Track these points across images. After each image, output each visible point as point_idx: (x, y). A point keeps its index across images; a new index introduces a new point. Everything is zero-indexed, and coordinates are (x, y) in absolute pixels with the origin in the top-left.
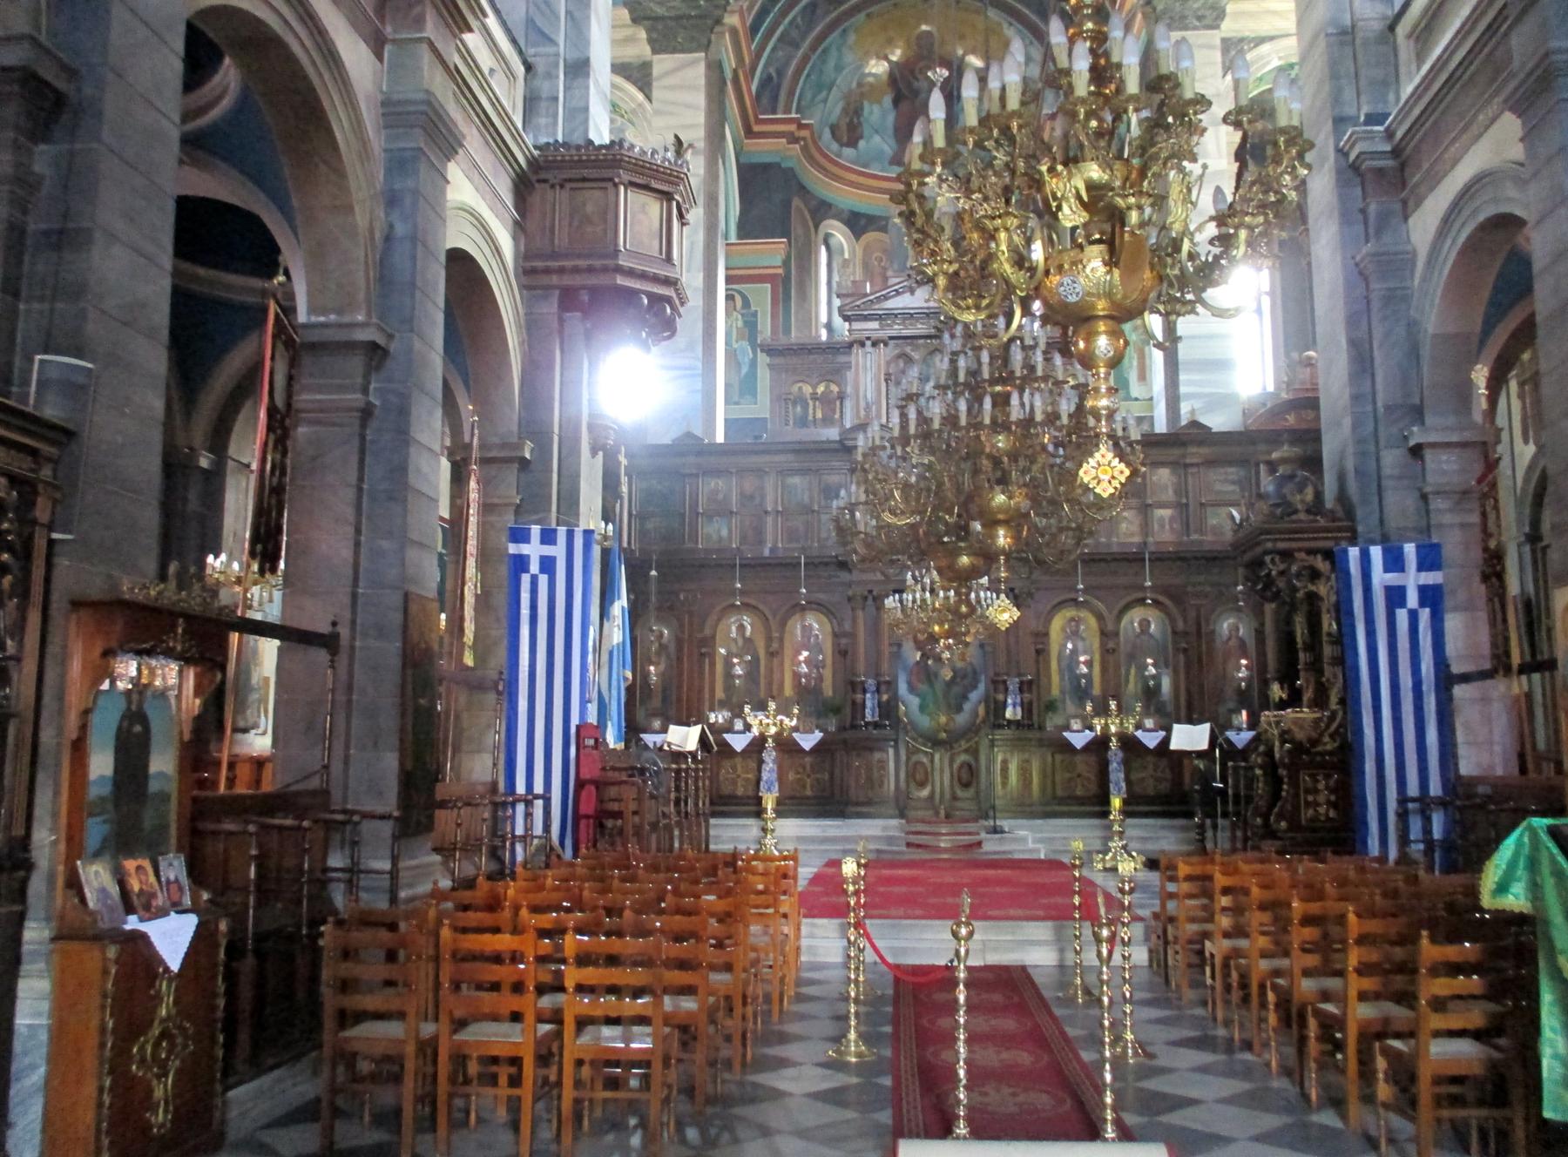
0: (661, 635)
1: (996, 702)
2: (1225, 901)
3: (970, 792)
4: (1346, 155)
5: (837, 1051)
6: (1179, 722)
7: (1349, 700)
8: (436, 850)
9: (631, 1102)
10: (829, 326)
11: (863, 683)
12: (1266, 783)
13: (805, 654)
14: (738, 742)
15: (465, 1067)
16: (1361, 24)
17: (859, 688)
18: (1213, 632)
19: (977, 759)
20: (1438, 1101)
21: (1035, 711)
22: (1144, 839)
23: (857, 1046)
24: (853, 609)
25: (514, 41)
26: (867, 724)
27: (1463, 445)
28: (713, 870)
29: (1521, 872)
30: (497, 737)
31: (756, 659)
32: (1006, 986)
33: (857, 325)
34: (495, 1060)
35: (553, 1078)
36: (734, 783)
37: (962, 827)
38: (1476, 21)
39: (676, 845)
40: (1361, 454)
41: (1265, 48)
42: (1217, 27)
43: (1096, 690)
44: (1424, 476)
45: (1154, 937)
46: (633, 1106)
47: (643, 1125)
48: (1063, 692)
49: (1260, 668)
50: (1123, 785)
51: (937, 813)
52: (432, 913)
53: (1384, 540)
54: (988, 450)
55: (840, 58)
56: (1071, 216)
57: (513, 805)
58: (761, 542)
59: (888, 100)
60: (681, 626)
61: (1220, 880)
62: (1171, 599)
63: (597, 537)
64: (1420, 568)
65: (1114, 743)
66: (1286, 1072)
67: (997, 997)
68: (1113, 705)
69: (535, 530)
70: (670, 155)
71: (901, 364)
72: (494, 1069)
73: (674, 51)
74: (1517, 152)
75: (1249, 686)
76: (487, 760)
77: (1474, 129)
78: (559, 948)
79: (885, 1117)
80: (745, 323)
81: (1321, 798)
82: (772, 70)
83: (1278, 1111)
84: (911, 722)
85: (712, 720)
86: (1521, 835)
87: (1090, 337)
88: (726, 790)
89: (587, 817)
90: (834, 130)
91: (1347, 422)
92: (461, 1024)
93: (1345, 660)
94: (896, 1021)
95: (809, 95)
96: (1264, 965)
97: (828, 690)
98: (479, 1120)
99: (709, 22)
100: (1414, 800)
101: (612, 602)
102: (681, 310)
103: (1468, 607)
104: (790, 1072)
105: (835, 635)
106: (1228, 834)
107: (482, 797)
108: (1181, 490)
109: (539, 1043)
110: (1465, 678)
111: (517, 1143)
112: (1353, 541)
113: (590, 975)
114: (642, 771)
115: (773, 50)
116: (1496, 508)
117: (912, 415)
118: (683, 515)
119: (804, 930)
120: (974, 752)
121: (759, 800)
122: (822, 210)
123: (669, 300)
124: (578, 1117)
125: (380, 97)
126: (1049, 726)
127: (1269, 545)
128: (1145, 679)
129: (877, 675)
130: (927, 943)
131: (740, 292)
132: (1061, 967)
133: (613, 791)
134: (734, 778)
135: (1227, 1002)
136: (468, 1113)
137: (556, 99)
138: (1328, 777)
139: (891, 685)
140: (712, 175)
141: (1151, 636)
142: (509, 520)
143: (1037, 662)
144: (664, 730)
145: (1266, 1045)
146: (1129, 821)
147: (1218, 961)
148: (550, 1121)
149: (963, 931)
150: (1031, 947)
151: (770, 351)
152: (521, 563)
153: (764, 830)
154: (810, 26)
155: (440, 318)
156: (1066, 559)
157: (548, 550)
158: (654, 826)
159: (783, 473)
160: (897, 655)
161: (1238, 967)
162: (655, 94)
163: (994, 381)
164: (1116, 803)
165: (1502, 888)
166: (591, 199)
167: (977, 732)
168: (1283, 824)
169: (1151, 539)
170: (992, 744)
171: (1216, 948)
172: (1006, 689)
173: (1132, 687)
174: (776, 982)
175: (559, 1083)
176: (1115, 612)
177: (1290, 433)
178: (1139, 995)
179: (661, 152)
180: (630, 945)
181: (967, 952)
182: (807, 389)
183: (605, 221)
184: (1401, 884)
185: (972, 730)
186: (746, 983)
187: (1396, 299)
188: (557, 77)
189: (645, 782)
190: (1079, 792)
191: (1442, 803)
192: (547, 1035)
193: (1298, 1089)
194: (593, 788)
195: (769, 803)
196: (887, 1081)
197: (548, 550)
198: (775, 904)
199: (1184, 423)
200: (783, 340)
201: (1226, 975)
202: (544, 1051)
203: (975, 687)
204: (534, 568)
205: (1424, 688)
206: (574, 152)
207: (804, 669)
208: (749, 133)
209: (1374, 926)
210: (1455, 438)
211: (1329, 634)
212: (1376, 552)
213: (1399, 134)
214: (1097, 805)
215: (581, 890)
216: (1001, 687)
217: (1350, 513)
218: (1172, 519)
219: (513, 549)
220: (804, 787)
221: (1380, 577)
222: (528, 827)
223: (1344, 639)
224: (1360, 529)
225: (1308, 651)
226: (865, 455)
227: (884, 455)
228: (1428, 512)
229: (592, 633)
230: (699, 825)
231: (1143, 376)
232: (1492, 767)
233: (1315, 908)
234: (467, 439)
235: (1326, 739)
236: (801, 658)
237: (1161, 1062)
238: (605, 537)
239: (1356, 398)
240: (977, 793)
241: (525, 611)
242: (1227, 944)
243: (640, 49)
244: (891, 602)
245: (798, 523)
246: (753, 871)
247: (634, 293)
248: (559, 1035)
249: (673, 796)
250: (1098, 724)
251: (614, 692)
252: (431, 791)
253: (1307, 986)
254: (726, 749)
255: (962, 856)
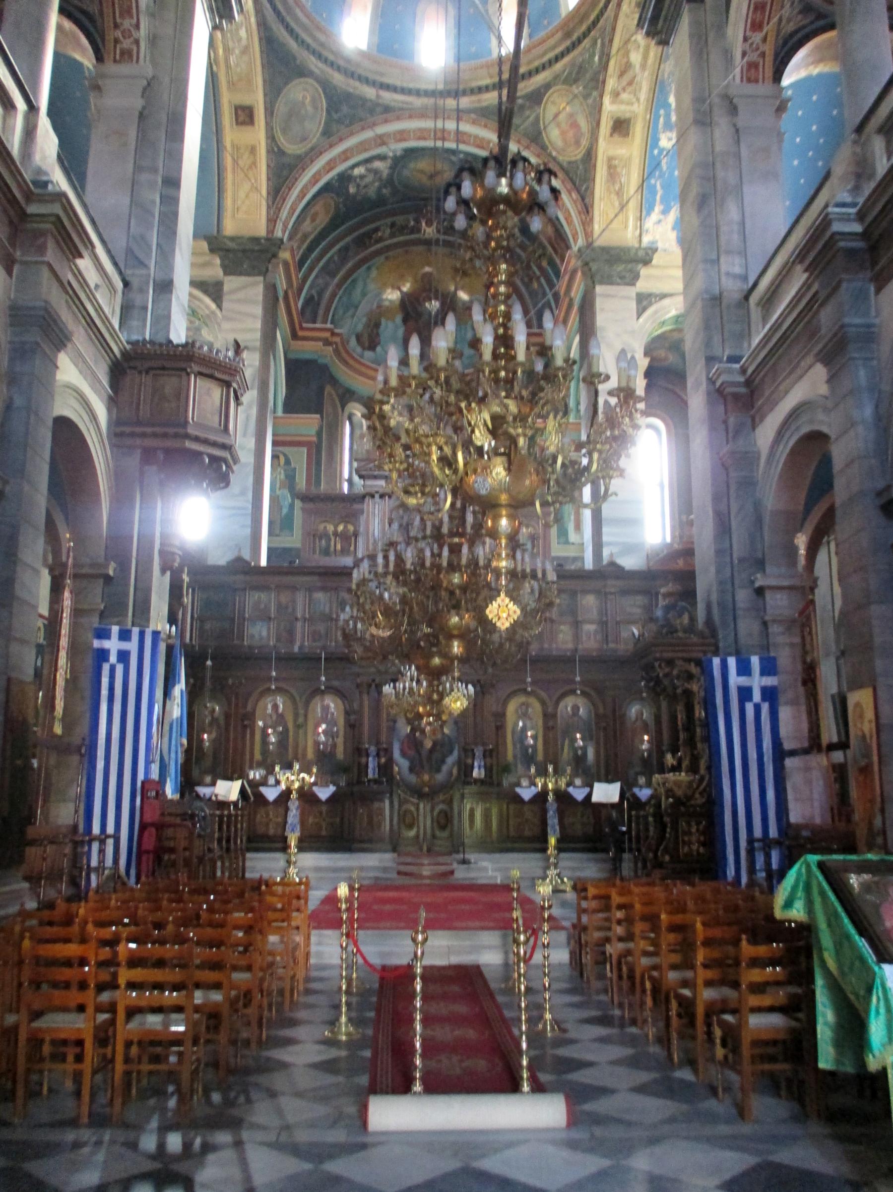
0: (214, 710)
1: (466, 765)
2: (619, 914)
3: (445, 834)
4: (714, 383)
5: (332, 1032)
6: (599, 781)
7: (714, 766)
8: (27, 878)
9: (170, 1073)
10: (350, 481)
11: (367, 750)
12: (655, 827)
13: (324, 726)
14: (271, 794)
15: (41, 1048)
16: (725, 294)
17: (364, 753)
18: (624, 715)
19: (452, 809)
20: (754, 1059)
21: (494, 772)
22: (573, 869)
23: (346, 1026)
24: (361, 693)
25: (115, 264)
26: (369, 781)
27: (790, 588)
28: (241, 895)
29: (800, 893)
30: (78, 789)
31: (286, 730)
32: (468, 978)
33: (369, 482)
34: (65, 1042)
35: (109, 1056)
36: (267, 825)
37: (441, 859)
38: (799, 300)
39: (219, 874)
40: (722, 592)
41: (666, 302)
42: (634, 284)
43: (540, 757)
44: (765, 608)
45: (572, 942)
46: (172, 1076)
47: (178, 1091)
48: (515, 756)
49: (657, 742)
50: (557, 828)
51: (421, 849)
52: (17, 928)
53: (737, 653)
54: (445, 585)
55: (365, 284)
56: (482, 439)
57: (90, 843)
58: (292, 641)
59: (399, 319)
60: (229, 704)
61: (616, 899)
62: (594, 691)
63: (162, 636)
64: (763, 673)
65: (551, 798)
66: (659, 1040)
67: (455, 988)
68: (550, 769)
69: (115, 629)
70: (231, 354)
71: (401, 512)
72: (63, 1049)
73: (241, 274)
74: (824, 389)
75: (649, 755)
76: (71, 807)
77: (799, 371)
78: (115, 954)
79: (364, 1080)
80: (287, 476)
81: (694, 838)
82: (314, 292)
83: (648, 1069)
84: (402, 779)
85: (251, 776)
86: (800, 869)
87: (496, 518)
88: (261, 830)
89: (148, 852)
90: (359, 338)
91: (713, 570)
92: (37, 1015)
93: (711, 738)
94: (378, 1010)
95: (341, 312)
96: (645, 961)
97: (340, 754)
98: (50, 1090)
99: (269, 255)
100: (759, 840)
101: (174, 685)
102: (235, 468)
103: (794, 703)
104: (291, 1049)
105: (347, 713)
106: (632, 865)
107: (65, 836)
108: (603, 612)
109: (98, 1029)
110: (793, 753)
111: (79, 1106)
112: (716, 653)
113: (138, 974)
114: (192, 816)
115: (316, 277)
116: (810, 633)
117: (392, 557)
118: (233, 620)
119: (313, 939)
120: (450, 802)
121: (285, 839)
122: (347, 395)
123: (225, 461)
124: (128, 1085)
125: (8, 303)
126: (505, 783)
127: (658, 655)
128: (575, 750)
129: (378, 743)
130: (392, 948)
131: (285, 455)
132: (506, 965)
133: (169, 832)
134: (266, 822)
135: (620, 989)
136: (41, 1085)
137: (146, 308)
138: (698, 824)
139: (388, 751)
140: (265, 366)
141: (580, 717)
142: (95, 621)
143: (497, 735)
144: (213, 784)
145: (645, 1021)
146: (562, 855)
147: (614, 962)
148: (106, 1090)
149: (420, 937)
150: (485, 951)
151: (305, 498)
152: (103, 655)
153: (289, 862)
154: (344, 259)
155: (46, 468)
156: (494, 663)
157: (125, 646)
158: (201, 860)
159: (310, 590)
160: (392, 729)
161: (627, 963)
162: (225, 305)
163: (452, 534)
164: (552, 841)
165: (788, 904)
166: (169, 384)
167: (451, 788)
168: (667, 858)
169: (580, 646)
170: (463, 797)
171: (613, 949)
172: (474, 755)
173: (566, 754)
174: (288, 981)
175: (112, 1061)
176: (555, 698)
177: (674, 575)
178: (555, 986)
179: (224, 352)
180: (171, 950)
181: (423, 953)
182: (331, 528)
183: (179, 399)
184: (740, 902)
185: (446, 787)
186: (262, 980)
187: (748, 484)
188: (148, 292)
189: (194, 825)
190: (527, 833)
191: (778, 843)
192: (105, 1021)
193: (666, 1053)
194: (153, 830)
195: (293, 843)
196: (367, 1053)
197: (125, 646)
198: (288, 919)
199: (605, 562)
200: (313, 490)
201: (620, 969)
202: (102, 1035)
203: (451, 752)
204: (113, 659)
205: (765, 759)
206: (157, 347)
207: (322, 738)
208: (295, 336)
209: (717, 932)
210: (786, 583)
211: (700, 720)
212: (732, 662)
213: (750, 371)
214: (538, 844)
215: (137, 908)
216: (470, 754)
217: (714, 633)
218: (596, 631)
219: (96, 644)
220: (320, 828)
221: (735, 680)
222: (102, 861)
223: (710, 723)
224: (721, 645)
225: (690, 732)
226: (358, 585)
227: (372, 585)
228: (767, 635)
229: (157, 709)
230: (237, 858)
231: (578, 527)
232: (812, 817)
233: (679, 919)
234: (64, 559)
235: (697, 795)
236: (320, 730)
237: (572, 1034)
238: (169, 636)
239: (719, 552)
240: (451, 835)
241: (104, 692)
242: (621, 946)
243: (215, 270)
244: (387, 689)
245: (321, 628)
246: (273, 894)
247: (199, 455)
248: (112, 1022)
249: (216, 835)
250: (540, 782)
251: (173, 755)
252: (22, 832)
253: (672, 976)
254: (261, 799)
255: (436, 882)
